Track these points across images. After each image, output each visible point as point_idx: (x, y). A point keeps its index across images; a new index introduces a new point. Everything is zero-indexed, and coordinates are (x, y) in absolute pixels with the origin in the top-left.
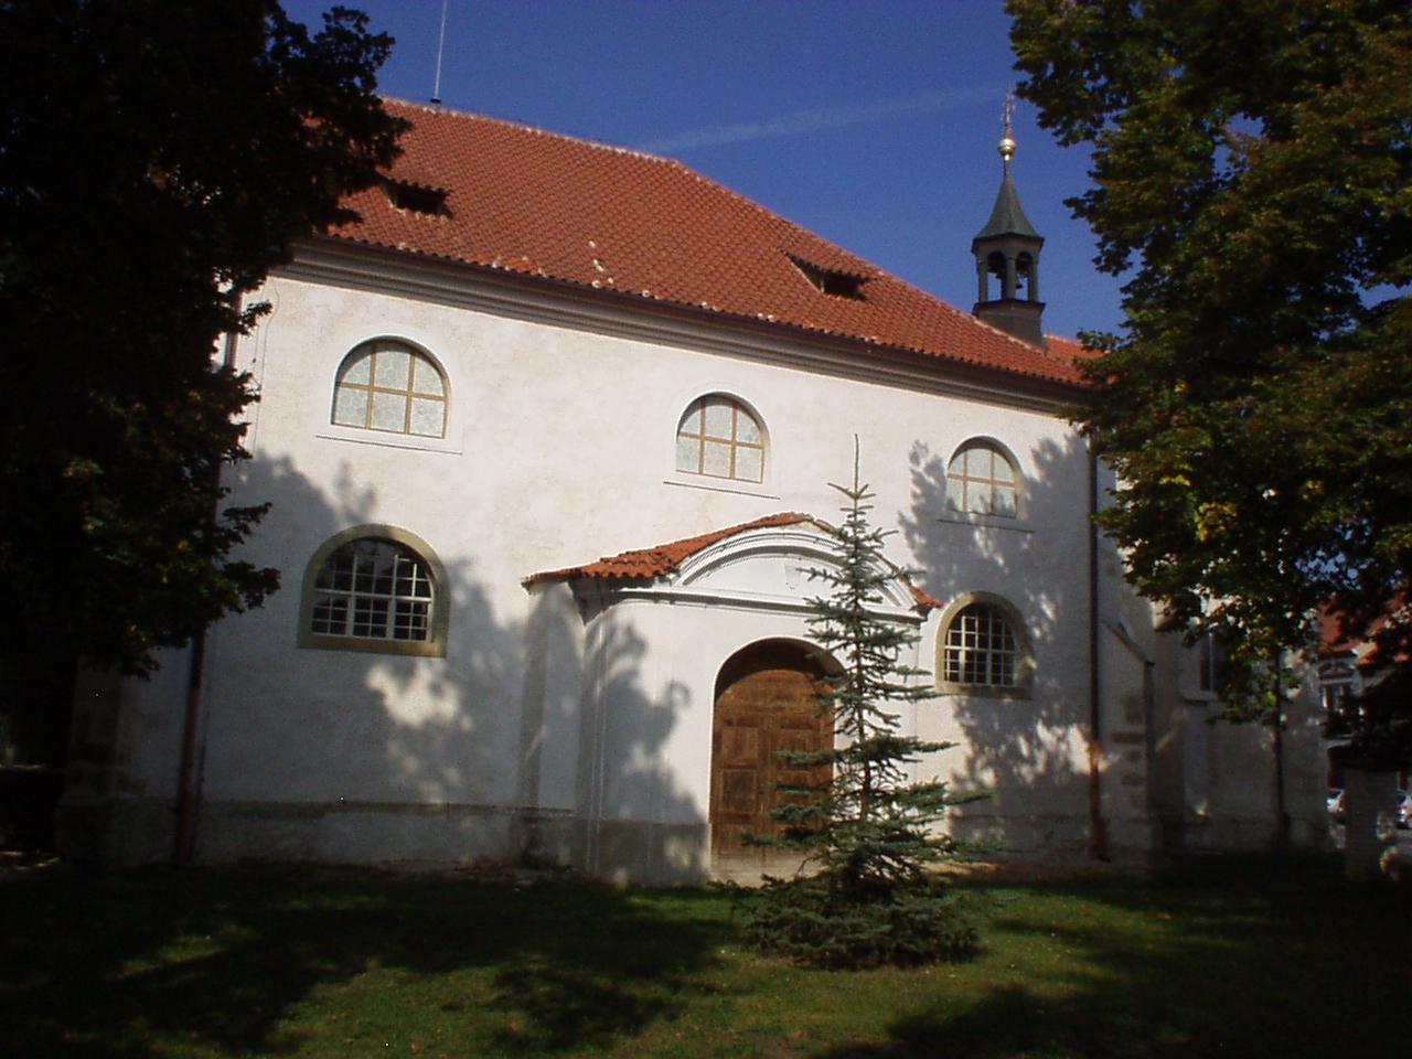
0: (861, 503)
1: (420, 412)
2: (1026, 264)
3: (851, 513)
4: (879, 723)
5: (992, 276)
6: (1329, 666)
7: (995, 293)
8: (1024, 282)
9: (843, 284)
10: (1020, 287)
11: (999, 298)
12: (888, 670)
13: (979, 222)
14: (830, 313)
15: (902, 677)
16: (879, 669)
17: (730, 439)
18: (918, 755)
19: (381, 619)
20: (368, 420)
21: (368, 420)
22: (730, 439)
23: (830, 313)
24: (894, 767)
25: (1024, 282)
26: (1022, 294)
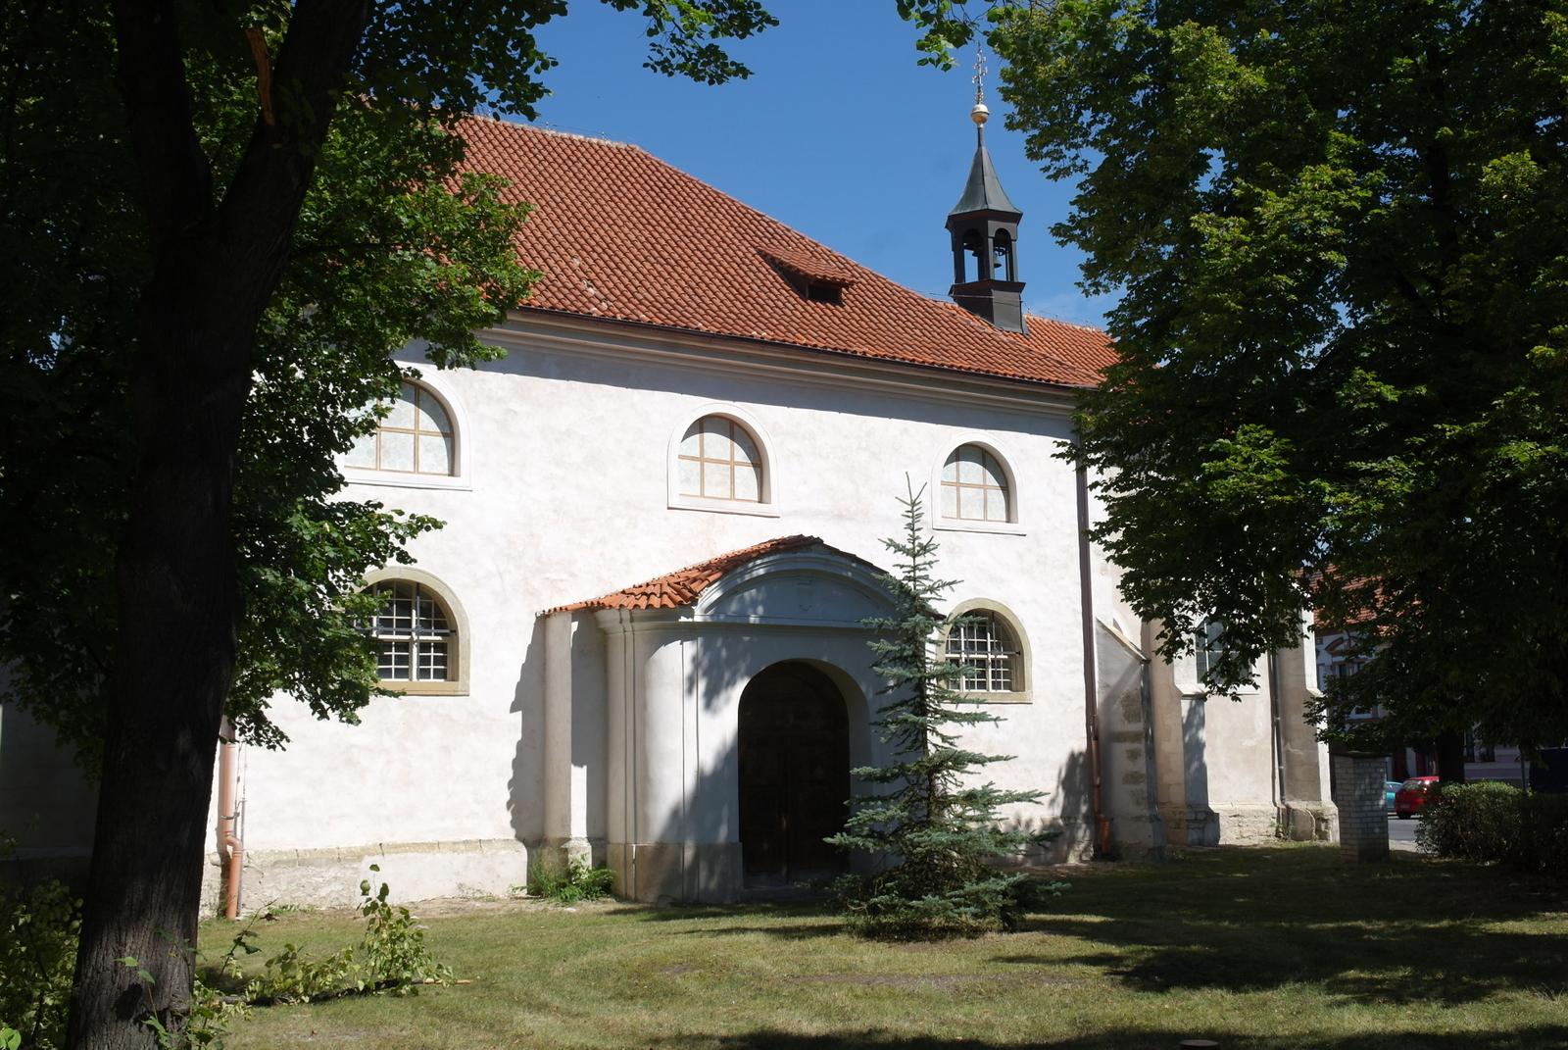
0: (919, 560)
1: (427, 450)
2: (1005, 241)
3: (909, 569)
4: (938, 741)
5: (968, 254)
6: (1341, 640)
7: (972, 275)
8: (1002, 259)
9: (824, 290)
10: (997, 266)
11: (977, 280)
12: (944, 698)
13: (951, 199)
14: (811, 324)
15: (975, 705)
16: (936, 697)
17: (728, 459)
18: (971, 767)
19: (405, 660)
20: (378, 459)
21: (378, 459)
22: (728, 459)
23: (811, 324)
24: (953, 776)
25: (1002, 259)
26: (1000, 274)
